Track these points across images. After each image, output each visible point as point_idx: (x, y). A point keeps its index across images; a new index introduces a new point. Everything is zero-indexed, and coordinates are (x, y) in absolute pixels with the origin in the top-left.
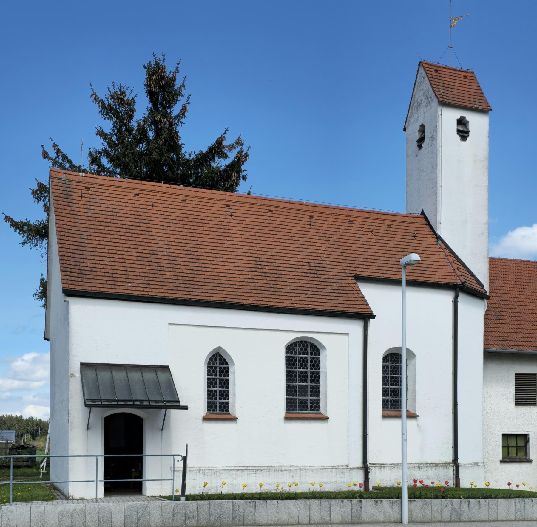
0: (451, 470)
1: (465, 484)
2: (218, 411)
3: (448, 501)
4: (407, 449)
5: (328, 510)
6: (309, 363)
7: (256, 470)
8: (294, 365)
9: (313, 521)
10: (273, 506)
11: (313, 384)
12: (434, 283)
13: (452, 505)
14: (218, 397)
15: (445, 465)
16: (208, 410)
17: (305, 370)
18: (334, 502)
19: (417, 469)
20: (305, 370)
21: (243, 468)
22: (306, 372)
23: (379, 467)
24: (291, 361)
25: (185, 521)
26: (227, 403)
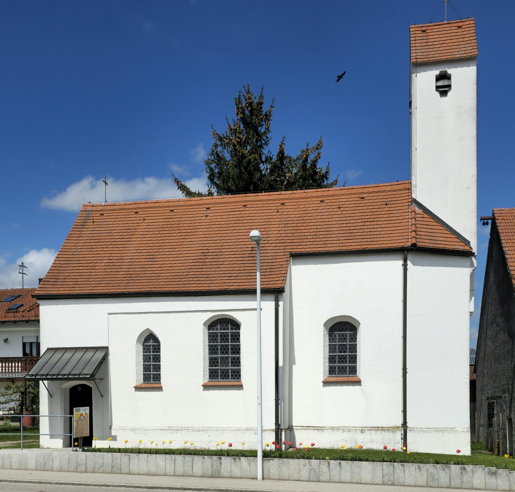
0: (399, 435)
1: (413, 447)
2: (152, 382)
3: (307, 461)
4: (325, 413)
5: (191, 465)
6: (230, 337)
7: (177, 430)
8: (216, 340)
9: (177, 473)
10: (144, 459)
11: (234, 356)
12: (360, 250)
13: (311, 466)
14: (152, 370)
15: (392, 429)
16: (144, 381)
17: (226, 343)
18: (196, 457)
19: (359, 432)
20: (226, 343)
21: (168, 428)
22: (227, 346)
23: (318, 430)
24: (213, 336)
25: (77, 467)
26: (159, 375)
